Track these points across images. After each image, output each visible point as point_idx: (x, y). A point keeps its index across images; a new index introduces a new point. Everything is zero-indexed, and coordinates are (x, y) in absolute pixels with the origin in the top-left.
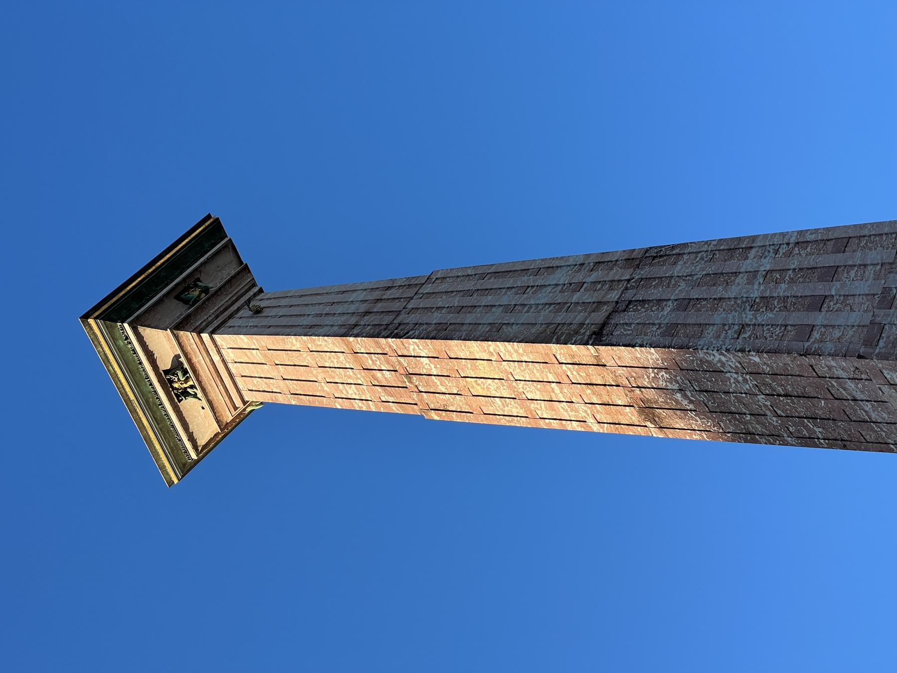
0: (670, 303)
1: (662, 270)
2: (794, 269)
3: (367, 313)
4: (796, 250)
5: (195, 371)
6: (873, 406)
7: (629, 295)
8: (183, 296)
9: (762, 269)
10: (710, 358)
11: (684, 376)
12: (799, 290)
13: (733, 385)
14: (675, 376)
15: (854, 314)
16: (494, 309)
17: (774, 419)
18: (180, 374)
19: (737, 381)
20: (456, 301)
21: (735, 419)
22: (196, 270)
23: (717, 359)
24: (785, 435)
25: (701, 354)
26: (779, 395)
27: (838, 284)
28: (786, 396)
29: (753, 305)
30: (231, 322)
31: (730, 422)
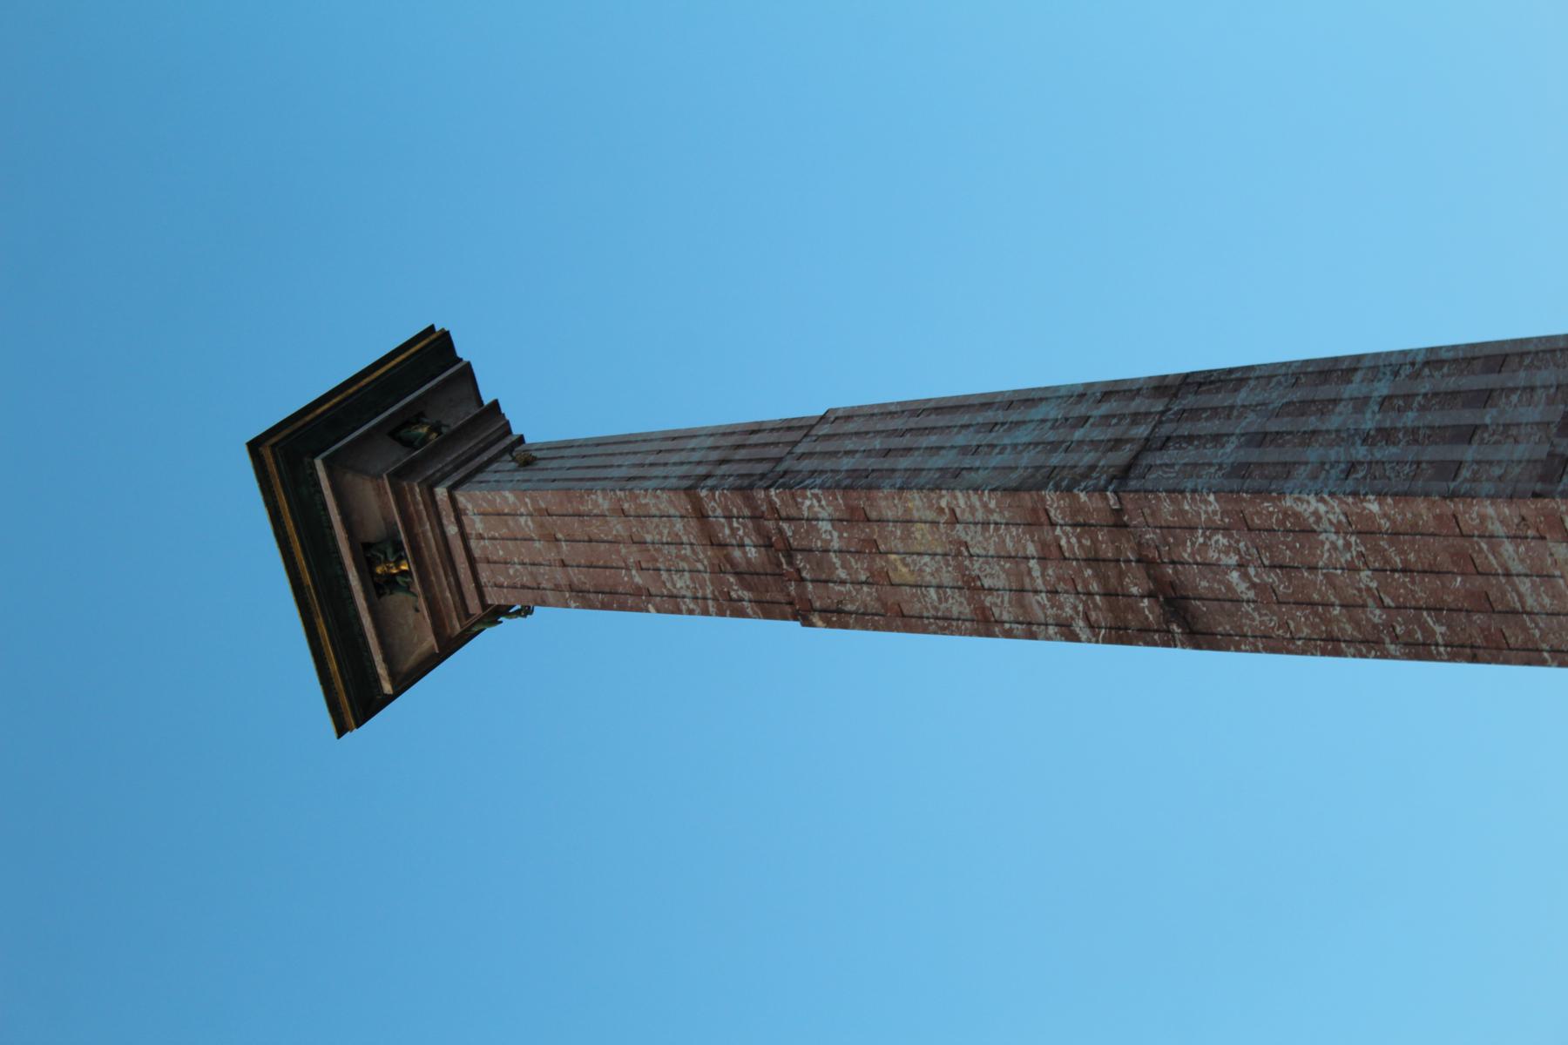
0: (1233, 439)
1: (1220, 399)
2: (1425, 395)
3: (722, 462)
4: (1426, 371)
5: (416, 550)
6: (1533, 584)
7: (1165, 430)
8: (403, 433)
9: (1376, 394)
10: (1300, 508)
11: (1253, 541)
12: (1435, 418)
13: (1326, 555)
14: (1238, 542)
15: (1521, 447)
16: (943, 452)
17: (1378, 612)
18: (390, 551)
19: (1334, 546)
20: (877, 443)
21: (1316, 614)
22: (419, 398)
23: (1311, 509)
24: (1387, 640)
25: (1288, 502)
26: (1394, 571)
27: (1494, 412)
28: (1404, 571)
29: (1366, 439)
30: (480, 477)
31: (1307, 618)
